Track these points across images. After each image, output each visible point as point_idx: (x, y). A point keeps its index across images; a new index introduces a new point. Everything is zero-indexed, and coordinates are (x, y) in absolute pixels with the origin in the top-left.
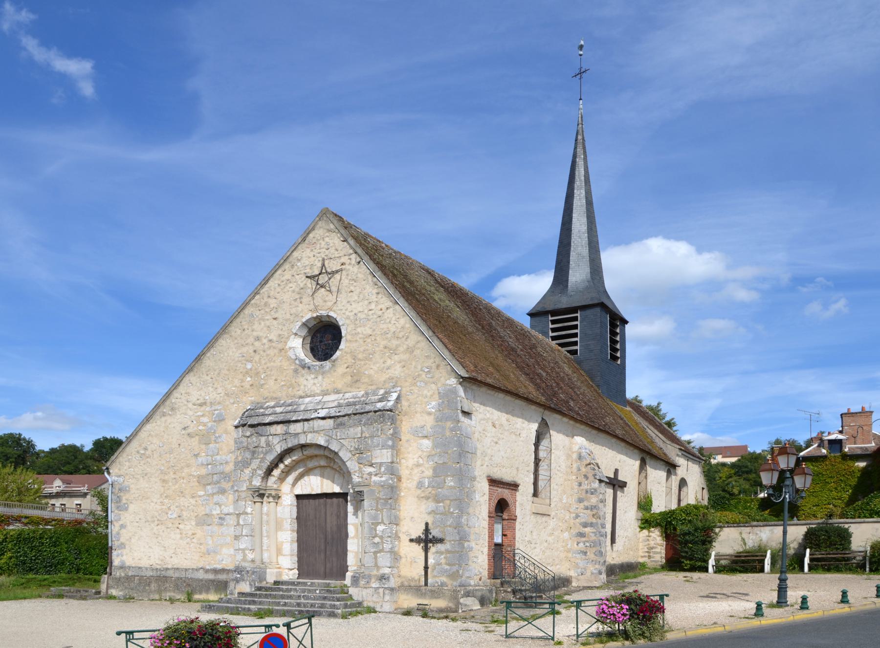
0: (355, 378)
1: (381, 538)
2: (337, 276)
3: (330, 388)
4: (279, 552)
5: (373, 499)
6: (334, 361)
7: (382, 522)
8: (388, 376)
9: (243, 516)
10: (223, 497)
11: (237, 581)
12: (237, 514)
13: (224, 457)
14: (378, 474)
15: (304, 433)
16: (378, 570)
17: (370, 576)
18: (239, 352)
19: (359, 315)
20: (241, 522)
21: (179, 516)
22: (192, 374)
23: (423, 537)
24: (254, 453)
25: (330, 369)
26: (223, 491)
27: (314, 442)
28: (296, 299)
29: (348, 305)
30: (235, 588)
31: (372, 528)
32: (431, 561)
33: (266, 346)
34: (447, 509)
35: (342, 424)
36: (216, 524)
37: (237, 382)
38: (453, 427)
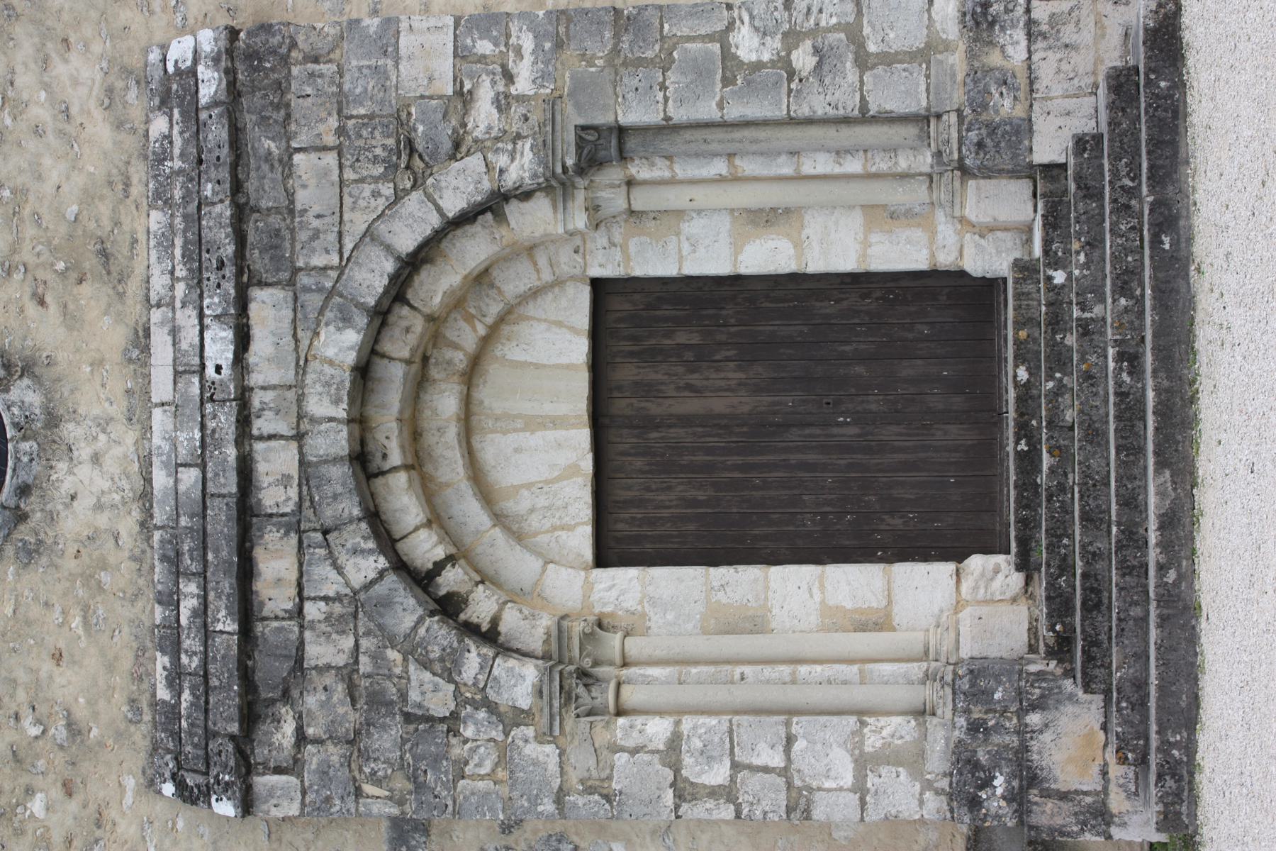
0: (91, 262)
1: (792, 38)
3: (119, 381)
7: (722, 37)
8: (98, 114)
9: (687, 760)
12: (680, 797)
14: (504, 67)
15: (299, 437)
16: (947, 47)
17: (977, 75)
20: (718, 775)
24: (377, 701)
30: (1064, 796)
31: (749, 83)
35: (273, 246)
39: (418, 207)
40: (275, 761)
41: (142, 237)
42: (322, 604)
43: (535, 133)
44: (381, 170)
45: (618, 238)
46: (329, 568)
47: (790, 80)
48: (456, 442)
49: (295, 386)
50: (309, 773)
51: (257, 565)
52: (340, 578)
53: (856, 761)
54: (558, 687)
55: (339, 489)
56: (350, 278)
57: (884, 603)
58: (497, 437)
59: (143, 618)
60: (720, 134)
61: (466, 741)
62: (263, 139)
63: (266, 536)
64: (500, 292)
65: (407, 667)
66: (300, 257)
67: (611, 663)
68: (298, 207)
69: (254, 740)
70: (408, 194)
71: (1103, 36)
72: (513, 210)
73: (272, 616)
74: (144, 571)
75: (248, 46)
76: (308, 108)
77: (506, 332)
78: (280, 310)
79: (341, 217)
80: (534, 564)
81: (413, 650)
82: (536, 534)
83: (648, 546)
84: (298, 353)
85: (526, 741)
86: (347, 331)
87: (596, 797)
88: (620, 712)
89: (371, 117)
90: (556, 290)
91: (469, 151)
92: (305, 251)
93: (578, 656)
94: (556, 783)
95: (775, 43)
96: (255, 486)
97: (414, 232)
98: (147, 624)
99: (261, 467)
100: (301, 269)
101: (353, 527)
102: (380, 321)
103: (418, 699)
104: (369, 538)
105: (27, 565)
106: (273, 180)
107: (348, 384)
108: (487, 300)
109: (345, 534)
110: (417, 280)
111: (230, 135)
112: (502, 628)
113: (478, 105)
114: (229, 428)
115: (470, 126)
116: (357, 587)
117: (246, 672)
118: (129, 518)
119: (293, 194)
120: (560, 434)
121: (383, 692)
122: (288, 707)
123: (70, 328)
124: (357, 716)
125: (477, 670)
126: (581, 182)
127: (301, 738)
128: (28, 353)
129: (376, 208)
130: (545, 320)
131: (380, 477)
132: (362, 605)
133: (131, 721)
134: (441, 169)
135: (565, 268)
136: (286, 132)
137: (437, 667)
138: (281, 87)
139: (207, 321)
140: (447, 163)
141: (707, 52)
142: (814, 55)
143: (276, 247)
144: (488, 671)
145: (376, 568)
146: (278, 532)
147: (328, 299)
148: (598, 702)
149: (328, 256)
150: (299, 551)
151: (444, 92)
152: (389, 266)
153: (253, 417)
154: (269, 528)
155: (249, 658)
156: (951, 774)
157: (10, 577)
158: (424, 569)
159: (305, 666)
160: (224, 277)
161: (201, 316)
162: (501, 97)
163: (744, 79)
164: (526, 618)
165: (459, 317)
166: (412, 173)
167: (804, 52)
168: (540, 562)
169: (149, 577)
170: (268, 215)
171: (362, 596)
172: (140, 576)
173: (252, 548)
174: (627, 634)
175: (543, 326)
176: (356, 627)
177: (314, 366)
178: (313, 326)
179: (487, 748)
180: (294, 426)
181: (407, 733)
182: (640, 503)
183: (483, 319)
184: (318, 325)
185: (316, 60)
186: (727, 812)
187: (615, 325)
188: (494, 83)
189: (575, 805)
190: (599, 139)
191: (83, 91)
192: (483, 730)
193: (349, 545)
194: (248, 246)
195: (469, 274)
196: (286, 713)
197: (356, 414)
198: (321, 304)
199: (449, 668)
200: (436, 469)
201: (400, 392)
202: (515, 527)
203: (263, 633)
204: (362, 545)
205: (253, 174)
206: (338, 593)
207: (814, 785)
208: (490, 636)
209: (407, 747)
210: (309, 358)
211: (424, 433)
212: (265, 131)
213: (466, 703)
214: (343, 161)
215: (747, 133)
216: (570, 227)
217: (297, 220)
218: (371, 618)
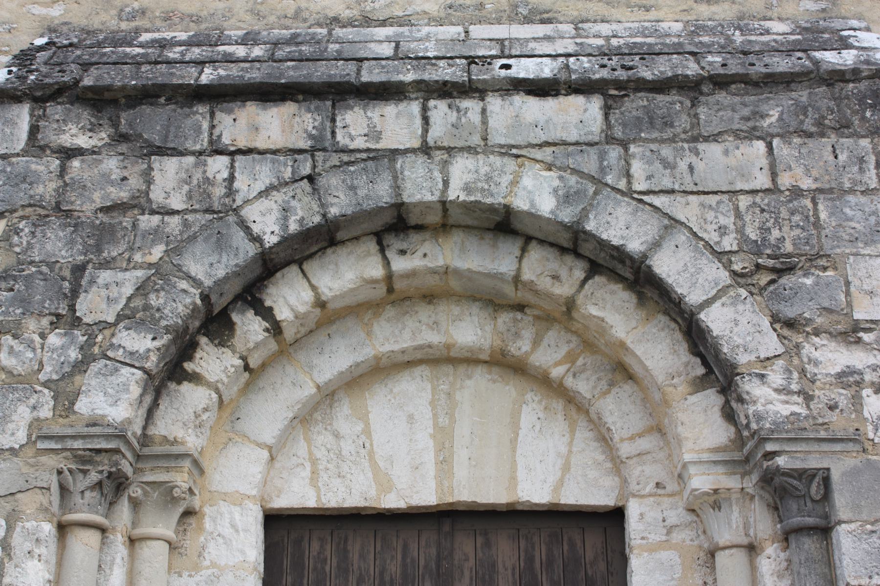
15: (425, 149)
27: (390, 260)
39: (710, 278)
40: (45, 127)
41: (653, 15)
42: (225, 174)
43: (814, 418)
44: (753, 236)
45: (677, 537)
46: (268, 182)
48: (421, 342)
49: (486, 145)
50: (27, 162)
51: (277, 106)
52: (255, 194)
54: (98, 447)
55: (361, 193)
56: (618, 203)
58: (427, 395)
59: (233, 21)
61: (43, 336)
62: (780, 109)
63: (309, 115)
64: (605, 394)
65: (141, 267)
66: (641, 149)
67: (134, 524)
68: (701, 146)
69: (72, 105)
70: (725, 267)
72: (711, 399)
73: (215, 122)
74: (283, 21)
76: (821, 157)
77: (554, 405)
78: (576, 127)
79: (692, 193)
80: (269, 435)
82: (308, 441)
83: (289, 579)
84: (526, 147)
85: (34, 408)
86: (554, 200)
88: (63, 528)
89: (817, 224)
90: (609, 465)
91: (785, 338)
92: (648, 153)
93: (145, 479)
96: (368, 104)
97: (679, 274)
98: (225, 24)
99: (390, 110)
100: (626, 150)
101: (316, 208)
102: (565, 244)
103: (100, 281)
104: (301, 225)
106: (731, 119)
107: (489, 200)
108: (594, 378)
109: (306, 199)
110: (618, 287)
111: (782, 74)
112: (186, 387)
113: (844, 351)
114: (437, 75)
115: (816, 340)
116: (243, 213)
117: (152, 96)
118: (343, 6)
119: (716, 141)
120: (430, 469)
121: (114, 241)
122: (107, 140)
124: (89, 214)
125: (129, 348)
126: (750, 483)
127: (68, 153)
129: (705, 230)
130: (570, 452)
131: (378, 247)
132: (221, 218)
133: (122, 10)
134: (759, 304)
135: (637, 472)
136: (791, 133)
137: (138, 303)
138: (843, 127)
140: (767, 312)
143: (652, 123)
144: (128, 361)
145: (265, 233)
146: (314, 128)
147: (592, 178)
148: (77, 499)
149: (643, 178)
150: (291, 150)
151: (856, 309)
152: (635, 246)
153: (449, 101)
154: (319, 118)
155: (169, 100)
158: (264, 297)
159: (153, 157)
160: (614, 70)
161: (569, 55)
162: (857, 377)
164: (197, 416)
165: (572, 345)
166: (751, 271)
168: (270, 441)
169: (277, 25)
170: (689, 114)
171: (232, 219)
172: (279, 18)
173: (297, 101)
174: (173, 547)
175: (564, 449)
176: (195, 211)
177: (511, 165)
178: (558, 163)
179: (31, 360)
180: (439, 143)
181: (61, 269)
182: (344, 570)
183: (570, 374)
184: (560, 169)
187: (565, 538)
190: (813, 501)
192: (55, 356)
193: (294, 203)
194: (651, 95)
195: (627, 349)
196: (103, 136)
197: (455, 216)
198: (586, 171)
200: (388, 320)
201: (481, 269)
202: (317, 416)
203: (197, 112)
204: (293, 218)
205: (737, 99)
206: (237, 191)
209: (44, 269)
210: (519, 160)
211: (432, 307)
212: (789, 111)
213: (90, 335)
214: (760, 194)
216: (692, 470)
217: (686, 145)
218: (203, 228)
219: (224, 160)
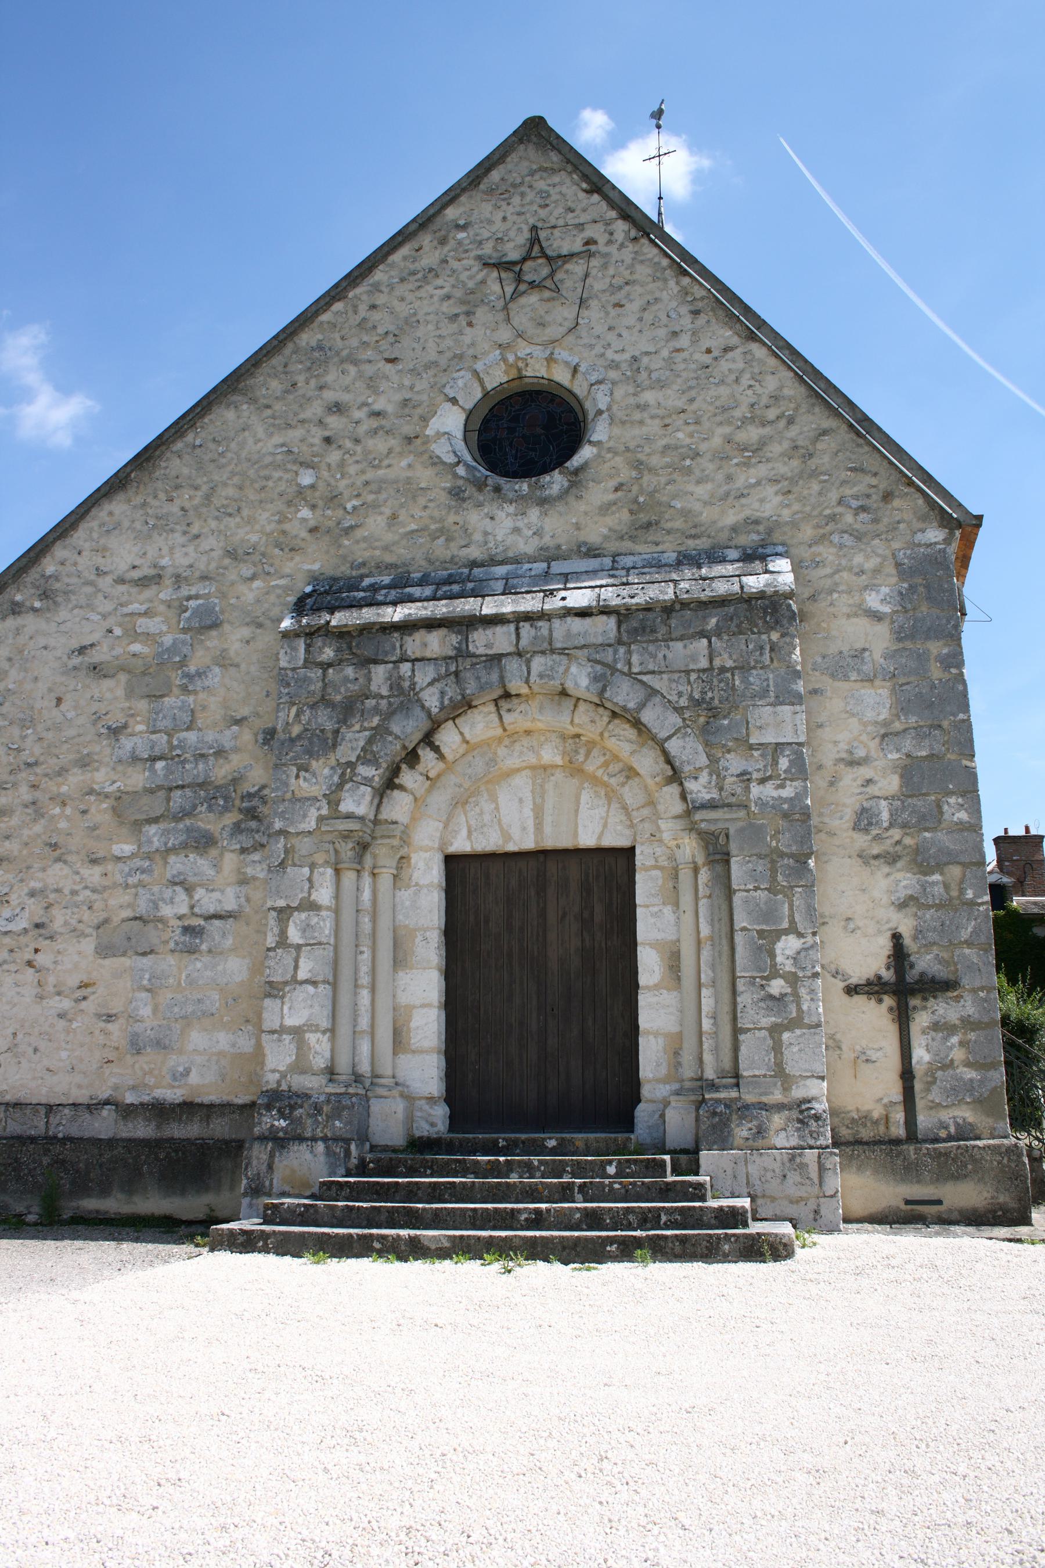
0: (643, 517)
1: (793, 980)
2: (577, 268)
4: (399, 1041)
5: (760, 856)
6: (577, 472)
7: (793, 929)
8: (742, 516)
9: (303, 915)
10: (201, 862)
11: (280, 1141)
12: (280, 911)
13: (210, 736)
14: (770, 778)
15: (519, 654)
16: (786, 1089)
18: (277, 439)
19: (645, 360)
20: (294, 935)
21: (38, 926)
22: (121, 496)
23: (888, 975)
25: (564, 493)
26: (203, 843)
28: (457, 315)
29: (611, 337)
30: (270, 1167)
31: (760, 948)
32: (920, 1055)
33: (362, 429)
34: (955, 893)
36: (172, 951)
37: (265, 518)
38: (948, 655)
44: (697, 697)
47: (762, 978)
53: (300, 1027)
57: (413, 1047)
60: (725, 929)
68: (671, 644)
71: (791, 1202)
75: (781, 605)
81: (380, 732)
85: (318, 809)
87: (283, 856)
94: (291, 830)
95: (789, 967)
99: (499, 630)
105: (450, 493)
109: (454, 686)
120: (531, 829)
123: (601, 508)
128: (584, 483)
139: (597, 590)
141: (782, 919)
142: (781, 994)
143: (644, 631)
156: (290, 1091)
157: (443, 485)
162: (748, 777)
163: (763, 945)
167: (783, 987)
177: (564, 660)
185: (772, 650)
186: (271, 941)
188: (759, 770)
189: (278, 842)
191: (756, 505)
193: (447, 689)
199: (367, 757)
207: (286, 1000)
208: (390, 784)
215: (726, 948)
219: (408, 665)
